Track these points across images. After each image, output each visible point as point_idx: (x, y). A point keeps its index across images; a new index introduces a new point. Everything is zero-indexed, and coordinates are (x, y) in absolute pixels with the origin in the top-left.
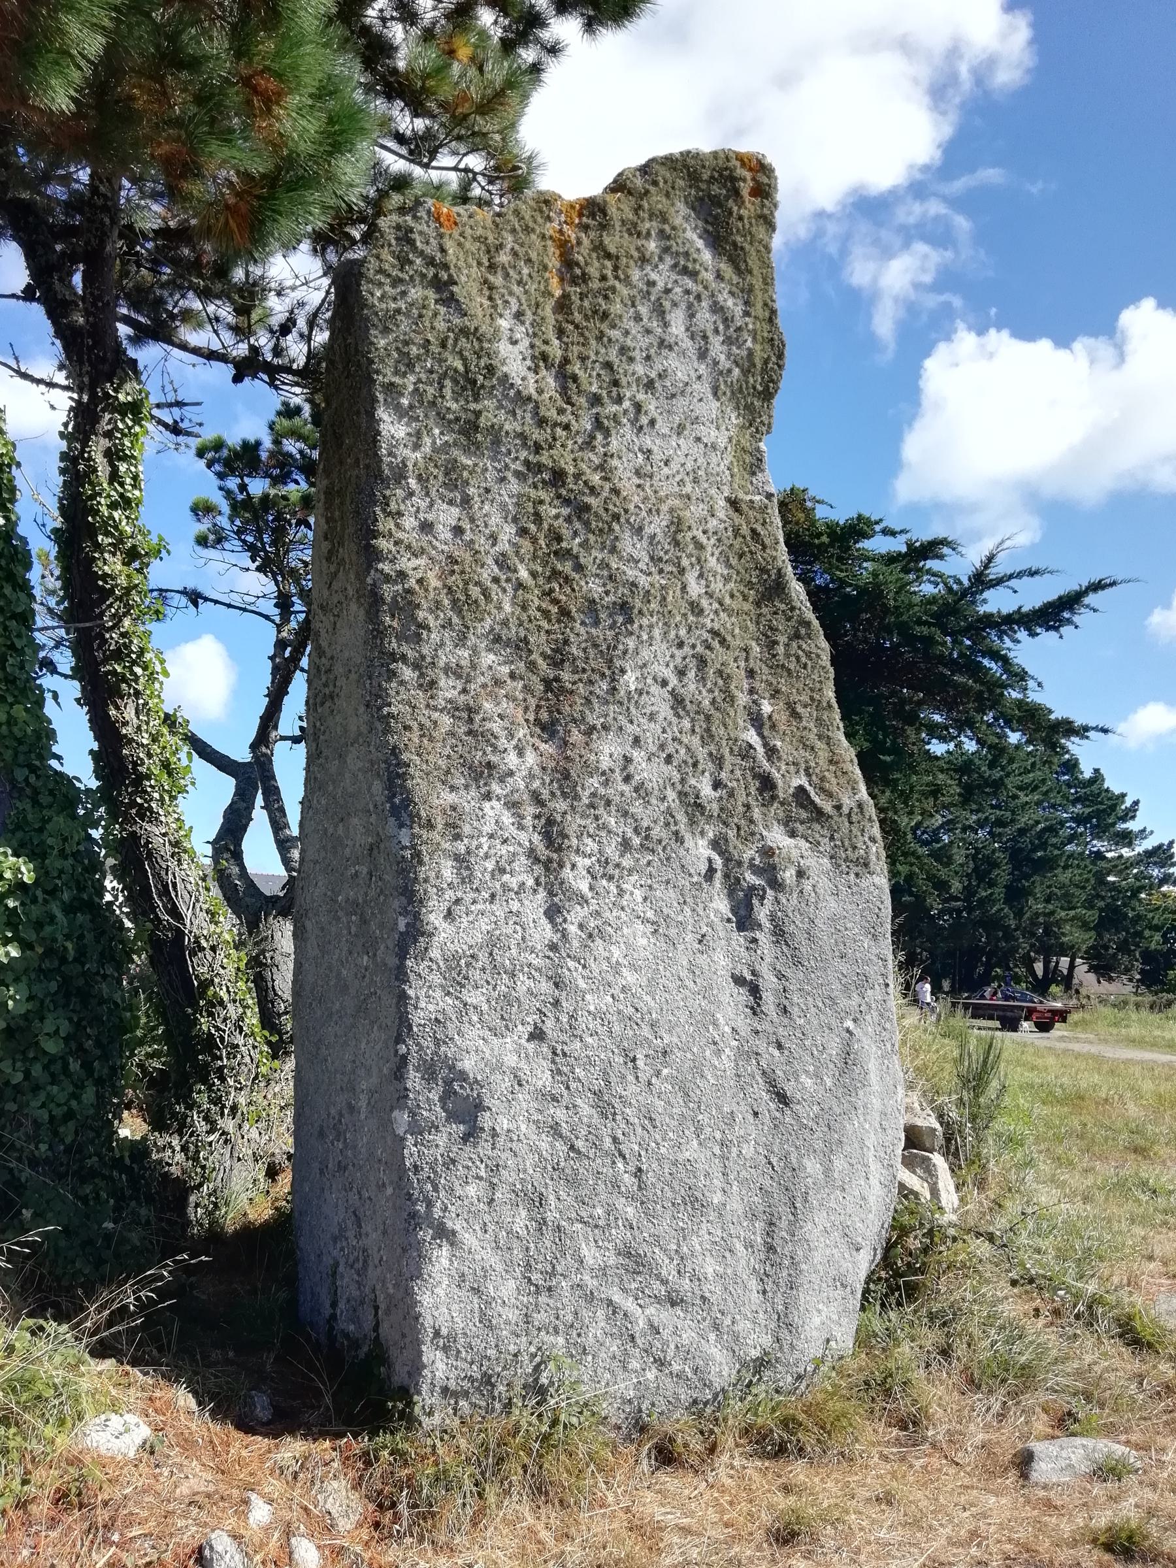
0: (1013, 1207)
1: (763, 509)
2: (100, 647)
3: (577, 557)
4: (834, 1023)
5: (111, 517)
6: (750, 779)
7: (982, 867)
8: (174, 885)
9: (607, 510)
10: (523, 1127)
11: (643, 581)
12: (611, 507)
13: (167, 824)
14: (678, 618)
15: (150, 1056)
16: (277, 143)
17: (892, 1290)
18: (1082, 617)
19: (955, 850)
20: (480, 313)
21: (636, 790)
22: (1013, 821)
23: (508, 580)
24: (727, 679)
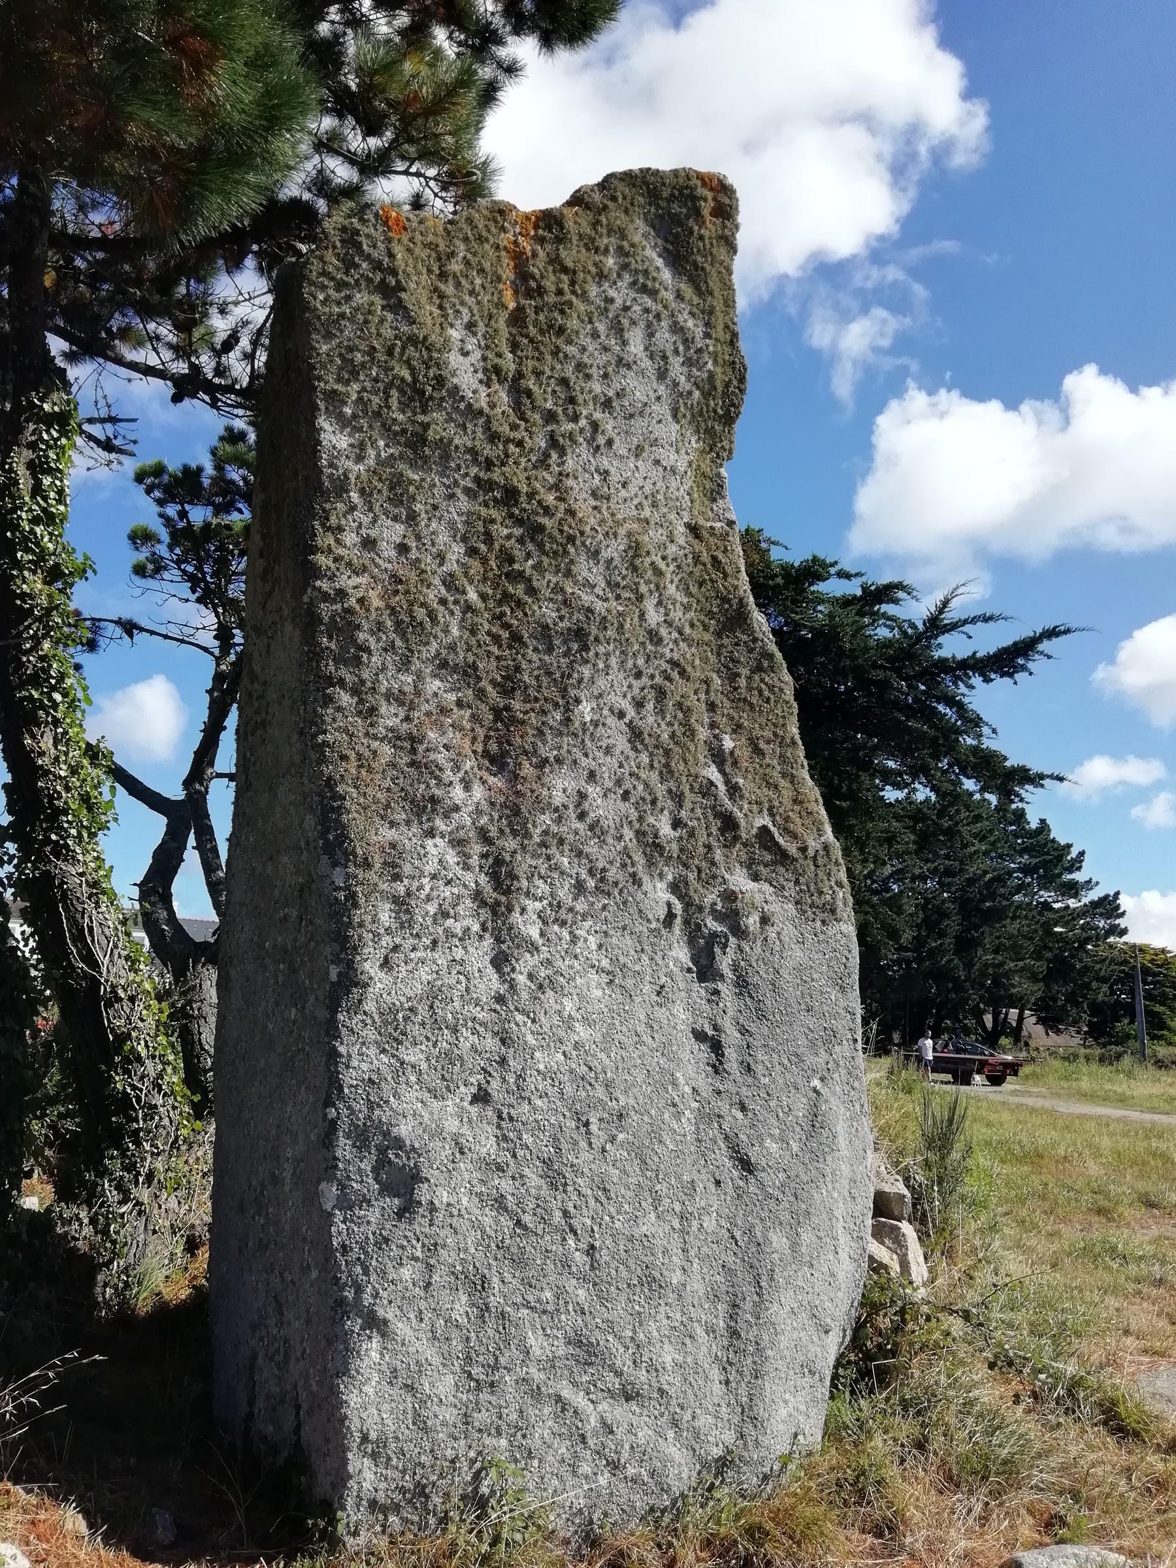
0: (984, 1277)
1: (724, 537)
2: (16, 670)
3: (530, 580)
4: (800, 1082)
5: (32, 532)
6: (711, 818)
7: (932, 918)
8: (91, 929)
9: (561, 531)
10: (465, 1201)
11: (599, 606)
12: (566, 528)
13: (85, 863)
14: (636, 647)
15: (61, 1116)
16: (207, 113)
17: (864, 1374)
18: (1037, 664)
19: (905, 900)
20: (429, 321)
21: (591, 828)
22: (961, 870)
23: (456, 602)
24: (687, 712)
